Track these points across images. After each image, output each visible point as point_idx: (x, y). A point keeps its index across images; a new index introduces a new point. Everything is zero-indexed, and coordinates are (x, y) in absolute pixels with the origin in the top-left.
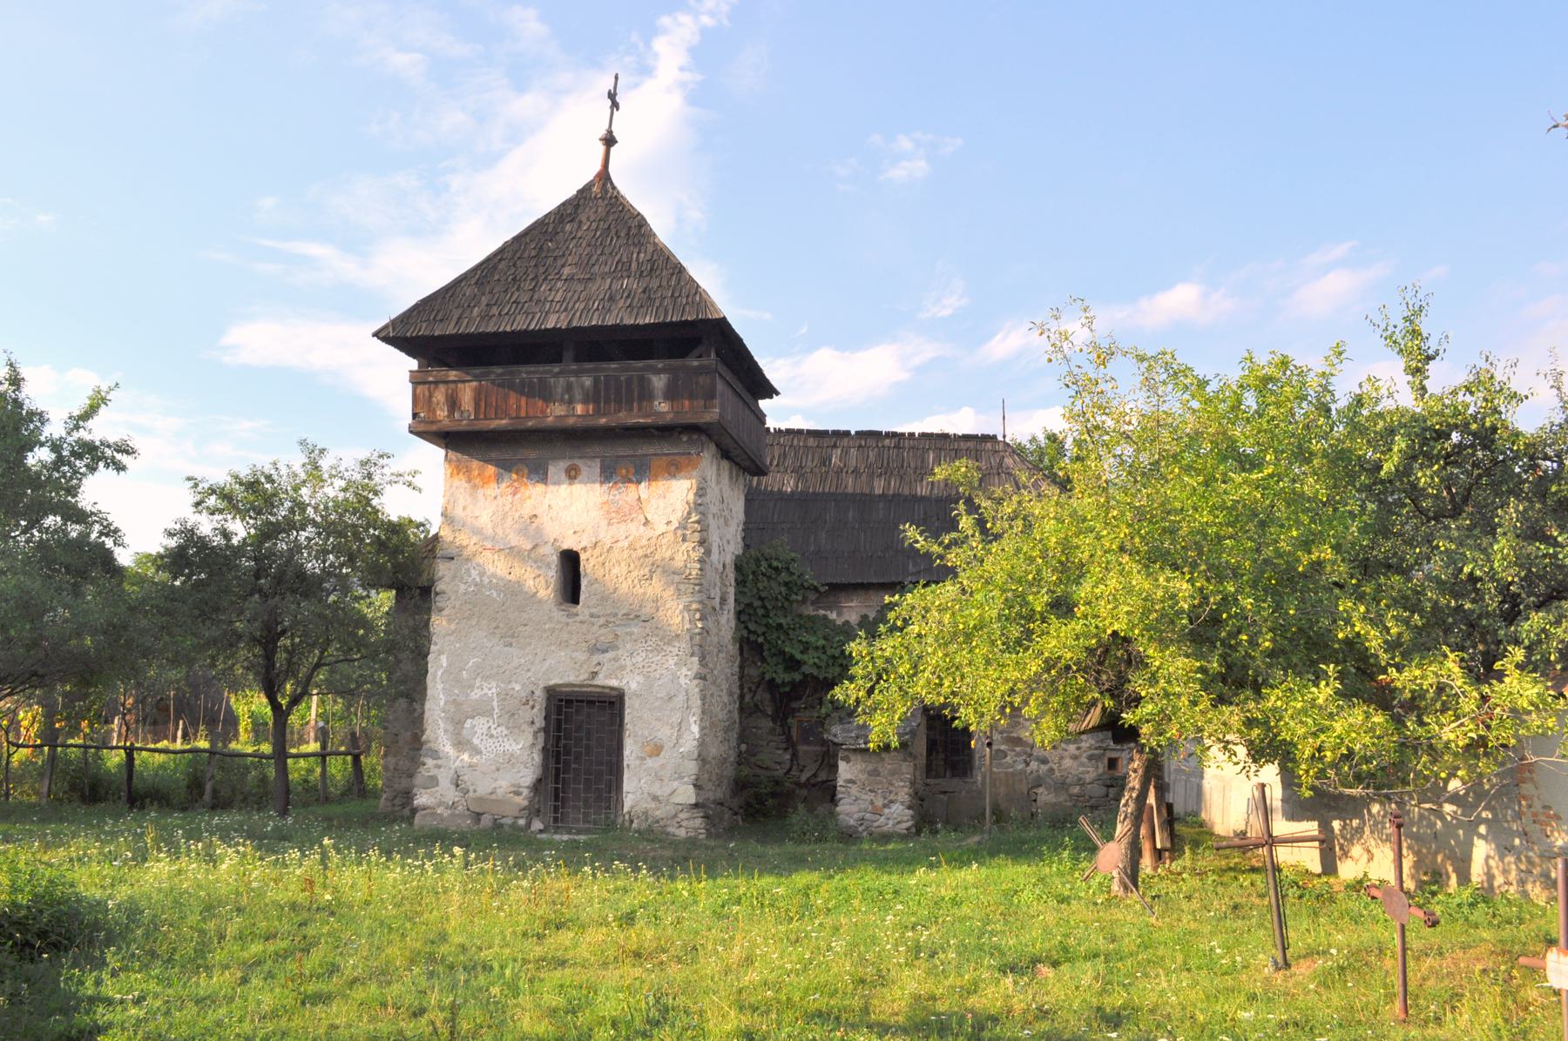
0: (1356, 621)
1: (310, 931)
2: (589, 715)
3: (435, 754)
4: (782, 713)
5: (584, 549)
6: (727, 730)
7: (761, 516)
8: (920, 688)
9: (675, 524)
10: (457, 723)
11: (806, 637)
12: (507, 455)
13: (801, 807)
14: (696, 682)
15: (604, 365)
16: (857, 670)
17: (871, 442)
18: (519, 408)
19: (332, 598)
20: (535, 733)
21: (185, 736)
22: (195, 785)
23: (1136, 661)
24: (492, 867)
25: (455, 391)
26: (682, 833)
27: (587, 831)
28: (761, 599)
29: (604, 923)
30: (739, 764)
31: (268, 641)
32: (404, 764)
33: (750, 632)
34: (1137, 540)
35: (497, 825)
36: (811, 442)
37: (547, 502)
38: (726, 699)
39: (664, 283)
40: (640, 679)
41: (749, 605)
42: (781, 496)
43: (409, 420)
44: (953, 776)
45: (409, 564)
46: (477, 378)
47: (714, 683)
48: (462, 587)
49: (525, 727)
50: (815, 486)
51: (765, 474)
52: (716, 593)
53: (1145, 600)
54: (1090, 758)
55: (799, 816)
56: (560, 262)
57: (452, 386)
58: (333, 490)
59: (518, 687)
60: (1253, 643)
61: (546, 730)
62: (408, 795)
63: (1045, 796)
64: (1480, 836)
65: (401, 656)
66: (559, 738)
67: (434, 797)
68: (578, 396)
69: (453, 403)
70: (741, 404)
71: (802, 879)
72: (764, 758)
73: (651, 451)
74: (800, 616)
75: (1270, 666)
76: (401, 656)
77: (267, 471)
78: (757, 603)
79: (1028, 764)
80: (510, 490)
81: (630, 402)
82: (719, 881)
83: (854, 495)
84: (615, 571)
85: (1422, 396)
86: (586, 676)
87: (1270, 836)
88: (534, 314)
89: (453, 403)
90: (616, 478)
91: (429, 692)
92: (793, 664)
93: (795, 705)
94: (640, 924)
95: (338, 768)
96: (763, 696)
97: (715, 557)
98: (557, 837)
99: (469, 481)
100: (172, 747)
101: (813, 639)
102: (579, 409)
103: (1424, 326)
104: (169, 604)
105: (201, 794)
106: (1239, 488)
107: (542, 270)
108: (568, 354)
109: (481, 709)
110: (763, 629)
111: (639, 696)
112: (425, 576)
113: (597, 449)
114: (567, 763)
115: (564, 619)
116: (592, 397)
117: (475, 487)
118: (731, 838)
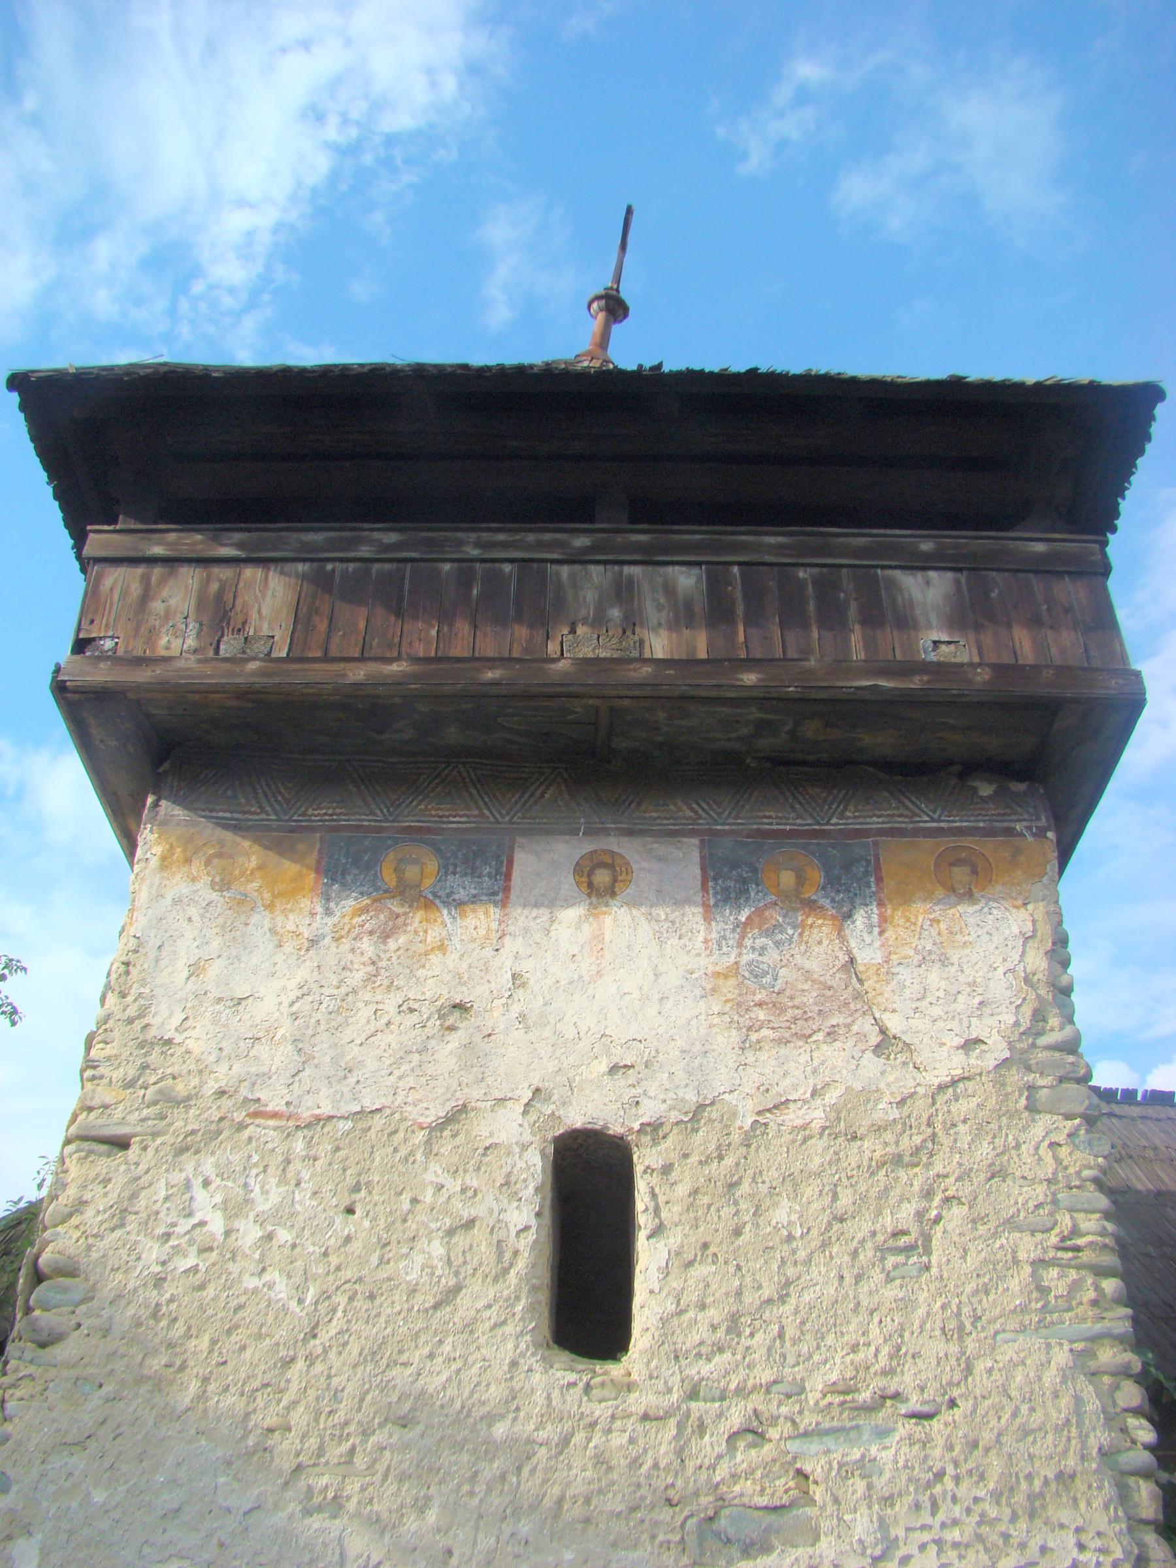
5: (654, 1129)
9: (997, 1050)
12: (365, 814)
37: (505, 963)
43: (63, 652)
57: (224, 573)
69: (220, 615)
84: (782, 1213)
99: (223, 884)
113: (683, 810)
117: (242, 904)
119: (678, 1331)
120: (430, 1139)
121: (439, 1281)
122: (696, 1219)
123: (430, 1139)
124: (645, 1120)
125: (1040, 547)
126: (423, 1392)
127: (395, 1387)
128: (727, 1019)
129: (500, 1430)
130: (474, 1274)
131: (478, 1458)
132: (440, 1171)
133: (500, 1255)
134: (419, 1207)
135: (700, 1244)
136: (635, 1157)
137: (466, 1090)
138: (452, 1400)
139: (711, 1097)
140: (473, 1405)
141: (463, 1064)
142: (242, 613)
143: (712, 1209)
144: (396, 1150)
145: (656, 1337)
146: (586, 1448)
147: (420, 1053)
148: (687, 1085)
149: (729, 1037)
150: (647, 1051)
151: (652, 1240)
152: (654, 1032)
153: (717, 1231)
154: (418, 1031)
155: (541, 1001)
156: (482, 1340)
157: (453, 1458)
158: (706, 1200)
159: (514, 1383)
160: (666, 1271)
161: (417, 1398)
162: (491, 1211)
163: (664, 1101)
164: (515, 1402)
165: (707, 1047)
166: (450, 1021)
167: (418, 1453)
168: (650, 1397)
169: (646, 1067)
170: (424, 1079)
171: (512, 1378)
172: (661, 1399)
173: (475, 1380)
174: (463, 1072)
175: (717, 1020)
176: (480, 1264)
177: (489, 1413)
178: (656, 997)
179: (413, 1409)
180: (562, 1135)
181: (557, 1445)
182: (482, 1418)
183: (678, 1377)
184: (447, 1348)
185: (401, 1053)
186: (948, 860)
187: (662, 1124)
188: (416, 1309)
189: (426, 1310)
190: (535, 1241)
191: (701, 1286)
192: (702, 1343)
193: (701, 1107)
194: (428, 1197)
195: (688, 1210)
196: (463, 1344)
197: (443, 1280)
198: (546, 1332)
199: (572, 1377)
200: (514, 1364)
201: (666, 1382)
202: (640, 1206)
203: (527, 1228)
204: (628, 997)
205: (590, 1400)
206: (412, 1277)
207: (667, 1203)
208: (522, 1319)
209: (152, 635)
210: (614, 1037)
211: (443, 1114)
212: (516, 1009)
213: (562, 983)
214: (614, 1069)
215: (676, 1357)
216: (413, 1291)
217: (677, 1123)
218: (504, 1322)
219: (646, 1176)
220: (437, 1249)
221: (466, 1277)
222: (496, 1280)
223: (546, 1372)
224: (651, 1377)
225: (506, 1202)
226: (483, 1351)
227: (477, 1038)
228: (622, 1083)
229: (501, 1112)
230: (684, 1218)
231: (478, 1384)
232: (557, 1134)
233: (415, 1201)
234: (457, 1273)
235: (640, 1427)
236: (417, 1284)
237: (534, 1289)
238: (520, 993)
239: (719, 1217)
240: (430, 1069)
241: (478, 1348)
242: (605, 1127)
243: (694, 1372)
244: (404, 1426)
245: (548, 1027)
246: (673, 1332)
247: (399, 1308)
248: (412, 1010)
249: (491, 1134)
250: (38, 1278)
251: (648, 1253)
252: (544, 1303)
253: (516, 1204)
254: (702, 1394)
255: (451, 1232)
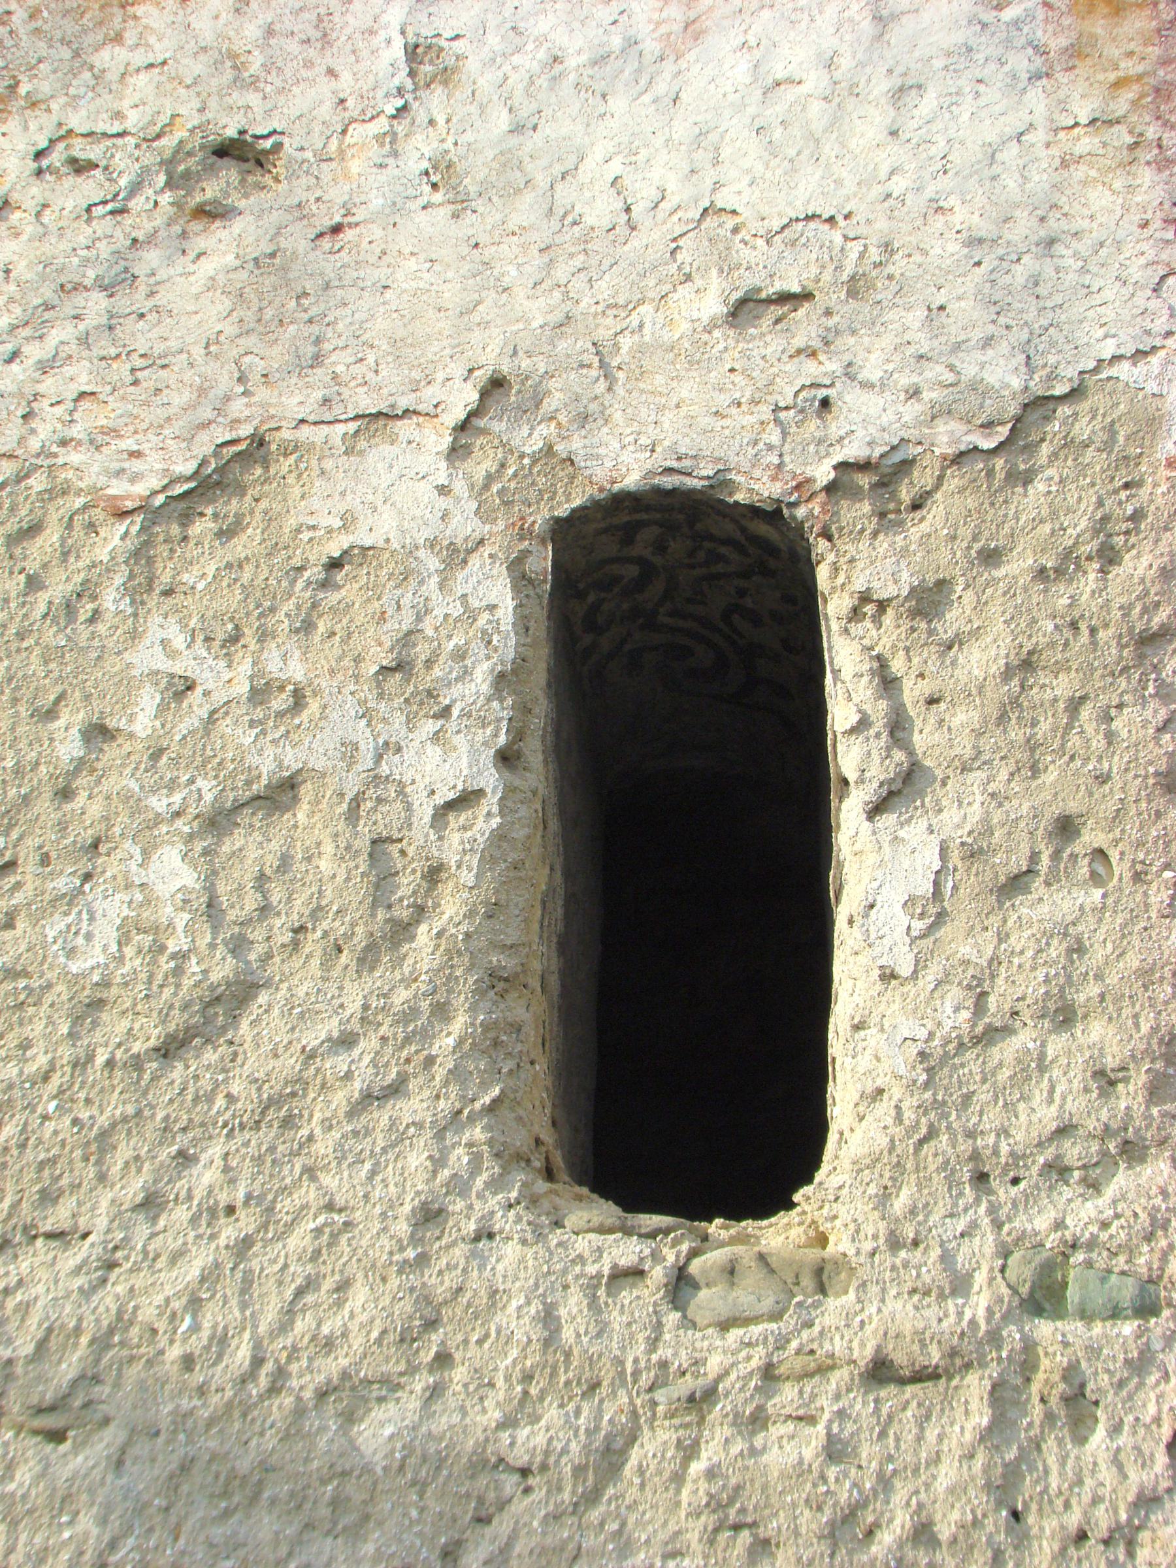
5: (881, 480)
119: (983, 1095)
120: (147, 544)
121: (178, 972)
122: (1031, 745)
123: (147, 544)
124: (853, 451)
126: (122, 1320)
127: (25, 1309)
128: (1121, 136)
129: (380, 1430)
130: (296, 945)
131: (309, 1526)
132: (179, 642)
133: (383, 882)
134: (111, 753)
135: (1046, 822)
136: (822, 574)
137: (262, 394)
138: (221, 1341)
139: (1071, 372)
140: (294, 1352)
141: (250, 316)
143: (1085, 713)
144: (34, 583)
145: (909, 1115)
146: (678, 1478)
147: (108, 288)
148: (988, 342)
149: (1131, 189)
150: (855, 248)
151: (888, 820)
152: (877, 191)
153: (1103, 779)
154: (103, 226)
155: (502, 121)
156: (324, 1147)
157: (218, 1532)
158: (1063, 686)
159: (430, 1276)
160: (934, 911)
161: (101, 1343)
162: (350, 751)
163: (914, 393)
164: (436, 1337)
165: (1055, 224)
166: (210, 190)
167: (103, 1521)
168: (892, 1305)
169: (852, 293)
170: (122, 370)
171: (423, 1260)
172: (932, 1313)
173: (299, 1271)
174: (251, 341)
175: (1086, 143)
176: (317, 912)
177: (345, 1375)
178: (882, 86)
179: (89, 1378)
180: (578, 517)
181: (579, 1471)
182: (322, 1394)
183: (985, 1243)
184: (205, 1176)
185: (48, 292)
187: (906, 465)
188: (101, 1059)
189: (137, 1063)
190: (499, 837)
191: (1056, 949)
192: (1063, 1131)
193: (1039, 405)
194: (142, 718)
195: (1003, 719)
196: (259, 1160)
197: (193, 966)
198: (538, 1120)
199: (626, 1251)
200: (430, 1215)
201: (946, 1258)
202: (840, 715)
203: (466, 799)
204: (790, 94)
205: (689, 1323)
206: (90, 960)
207: (932, 701)
208: (455, 1074)
210: (746, 213)
211: (189, 468)
212: (420, 149)
213: (572, 62)
214: (744, 309)
215: (981, 1178)
216: (91, 1007)
217: (959, 458)
218: (396, 1090)
219: (856, 629)
220: (173, 872)
221: (269, 956)
222: (367, 959)
223: (540, 1237)
224: (895, 1243)
225: (399, 720)
226: (328, 1180)
227: (297, 240)
228: (775, 345)
229: (379, 456)
230: (987, 743)
231: (309, 1285)
232: (562, 511)
233: (99, 733)
234: (238, 946)
235: (861, 1405)
236: (105, 984)
237: (497, 984)
238: (435, 102)
239: (1110, 737)
240: (143, 337)
241: (310, 1172)
242: (721, 482)
243: (1042, 1223)
244: (57, 1436)
245: (528, 197)
246: (967, 1098)
247: (43, 1060)
248: (79, 167)
249: (348, 521)
251: (872, 859)
252: (531, 1034)
253: (431, 726)
254: (1072, 1294)
255: (218, 822)
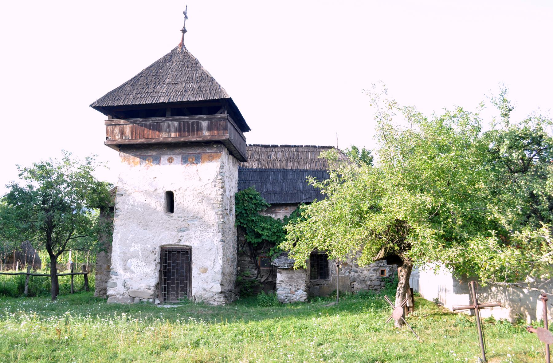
0: (494, 212)
1: (58, 353)
2: (178, 257)
3: (116, 274)
4: (253, 256)
5: (175, 191)
6: (233, 262)
7: (244, 178)
8: (316, 244)
10: (125, 261)
11: (263, 225)
13: (263, 292)
14: (221, 243)
15: (183, 117)
16: (288, 237)
17: (286, 149)
18: (149, 134)
19: (75, 212)
20: (156, 264)
21: (19, 268)
22: (21, 287)
23: (409, 231)
24: (137, 323)
25: (123, 128)
26: (216, 304)
27: (178, 304)
28: (245, 210)
29: (185, 346)
30: (237, 275)
31: (49, 227)
32: (104, 278)
33: (241, 223)
34: (405, 180)
35: (141, 302)
36: (263, 149)
38: (232, 249)
39: (206, 85)
40: (198, 242)
41: (241, 212)
42: (252, 170)
44: (321, 278)
45: (106, 201)
46: (132, 123)
47: (227, 243)
48: (126, 207)
49: (152, 262)
50: (265, 166)
51: (246, 161)
52: (228, 207)
53: (412, 204)
54: (374, 270)
55: (262, 296)
56: (165, 77)
57: (122, 126)
58: (74, 169)
59: (149, 246)
60: (454, 222)
61: (160, 263)
62: (105, 290)
63: (357, 285)
64: (539, 300)
65: (103, 234)
66: (166, 266)
67: (116, 291)
68: (172, 129)
69: (122, 133)
70: (237, 133)
71: (267, 323)
72: (247, 272)
73: (202, 151)
74: (261, 216)
75: (462, 232)
76: (103, 234)
77: (48, 162)
78: (244, 212)
79: (350, 273)
80: (146, 167)
81: (193, 131)
82: (232, 324)
83: (280, 169)
85: (508, 125)
86: (176, 241)
87: (482, 308)
88: (155, 97)
89: (122, 133)
90: (188, 162)
91: (113, 249)
92: (258, 235)
93: (259, 252)
94: (201, 346)
95: (78, 280)
96: (246, 248)
97: (227, 193)
98: (165, 306)
100: (14, 272)
101: (266, 226)
102: (173, 135)
103: (507, 97)
104: (6, 215)
105: (23, 291)
106: (443, 160)
107: (158, 80)
108: (168, 113)
109: (134, 256)
110: (246, 222)
111: (198, 249)
112: (112, 203)
113: (180, 151)
114: (169, 276)
115: (168, 219)
116: (179, 130)
118: (236, 304)
125: (219, 116)
142: (127, 130)
186: (209, 156)
209: (115, 137)
250: (116, 209)
